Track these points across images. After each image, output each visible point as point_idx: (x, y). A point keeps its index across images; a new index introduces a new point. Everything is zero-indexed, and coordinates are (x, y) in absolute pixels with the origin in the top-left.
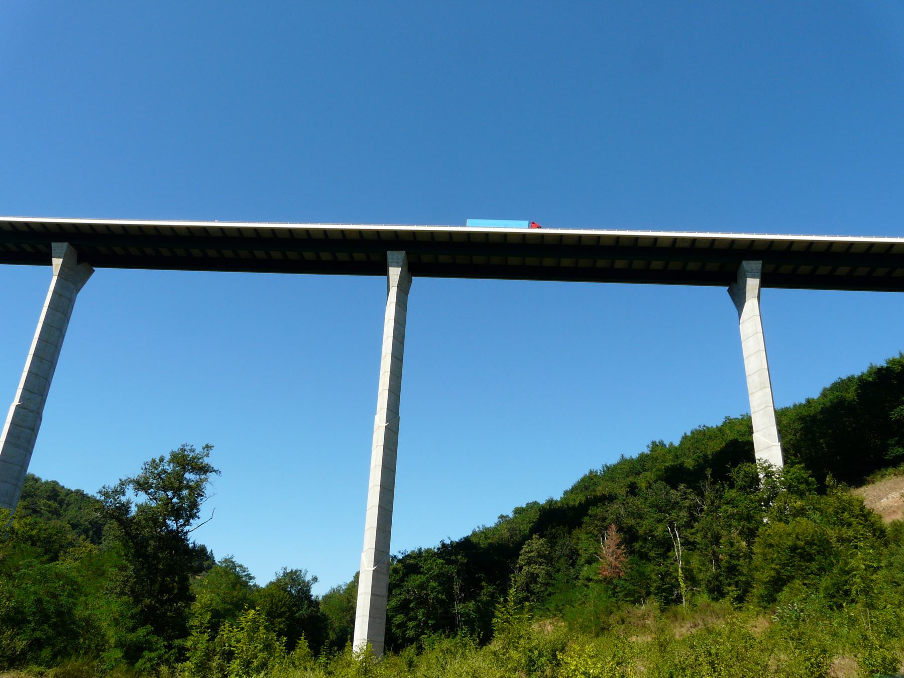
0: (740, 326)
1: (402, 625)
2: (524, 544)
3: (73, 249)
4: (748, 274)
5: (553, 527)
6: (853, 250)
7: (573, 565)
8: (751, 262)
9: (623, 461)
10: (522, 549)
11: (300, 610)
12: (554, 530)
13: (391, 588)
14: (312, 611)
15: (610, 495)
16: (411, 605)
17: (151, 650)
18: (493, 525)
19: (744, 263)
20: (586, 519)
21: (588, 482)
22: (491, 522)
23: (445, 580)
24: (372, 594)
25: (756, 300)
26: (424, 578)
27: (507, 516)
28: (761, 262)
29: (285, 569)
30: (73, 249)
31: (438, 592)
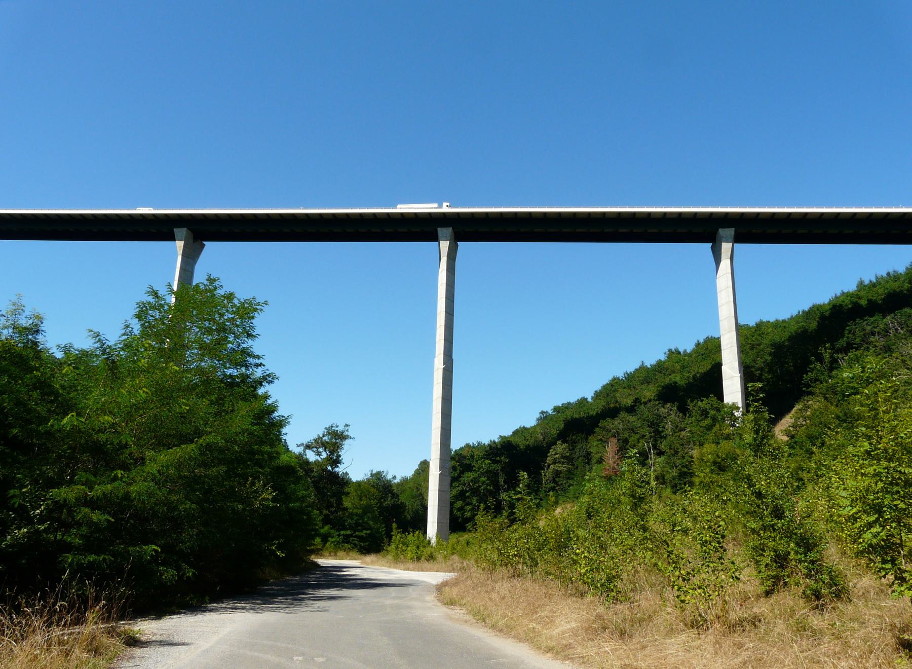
1: (461, 509)
2: (550, 449)
4: (724, 239)
5: (574, 434)
6: (807, 217)
7: (588, 463)
9: (642, 368)
11: (385, 501)
13: (454, 480)
16: (467, 494)
17: (332, 537)
19: (720, 230)
20: (597, 430)
21: (613, 386)
22: (530, 421)
23: (492, 476)
24: (439, 490)
25: (729, 261)
26: (476, 475)
27: (547, 412)
28: (734, 229)
29: (372, 471)
31: (487, 485)
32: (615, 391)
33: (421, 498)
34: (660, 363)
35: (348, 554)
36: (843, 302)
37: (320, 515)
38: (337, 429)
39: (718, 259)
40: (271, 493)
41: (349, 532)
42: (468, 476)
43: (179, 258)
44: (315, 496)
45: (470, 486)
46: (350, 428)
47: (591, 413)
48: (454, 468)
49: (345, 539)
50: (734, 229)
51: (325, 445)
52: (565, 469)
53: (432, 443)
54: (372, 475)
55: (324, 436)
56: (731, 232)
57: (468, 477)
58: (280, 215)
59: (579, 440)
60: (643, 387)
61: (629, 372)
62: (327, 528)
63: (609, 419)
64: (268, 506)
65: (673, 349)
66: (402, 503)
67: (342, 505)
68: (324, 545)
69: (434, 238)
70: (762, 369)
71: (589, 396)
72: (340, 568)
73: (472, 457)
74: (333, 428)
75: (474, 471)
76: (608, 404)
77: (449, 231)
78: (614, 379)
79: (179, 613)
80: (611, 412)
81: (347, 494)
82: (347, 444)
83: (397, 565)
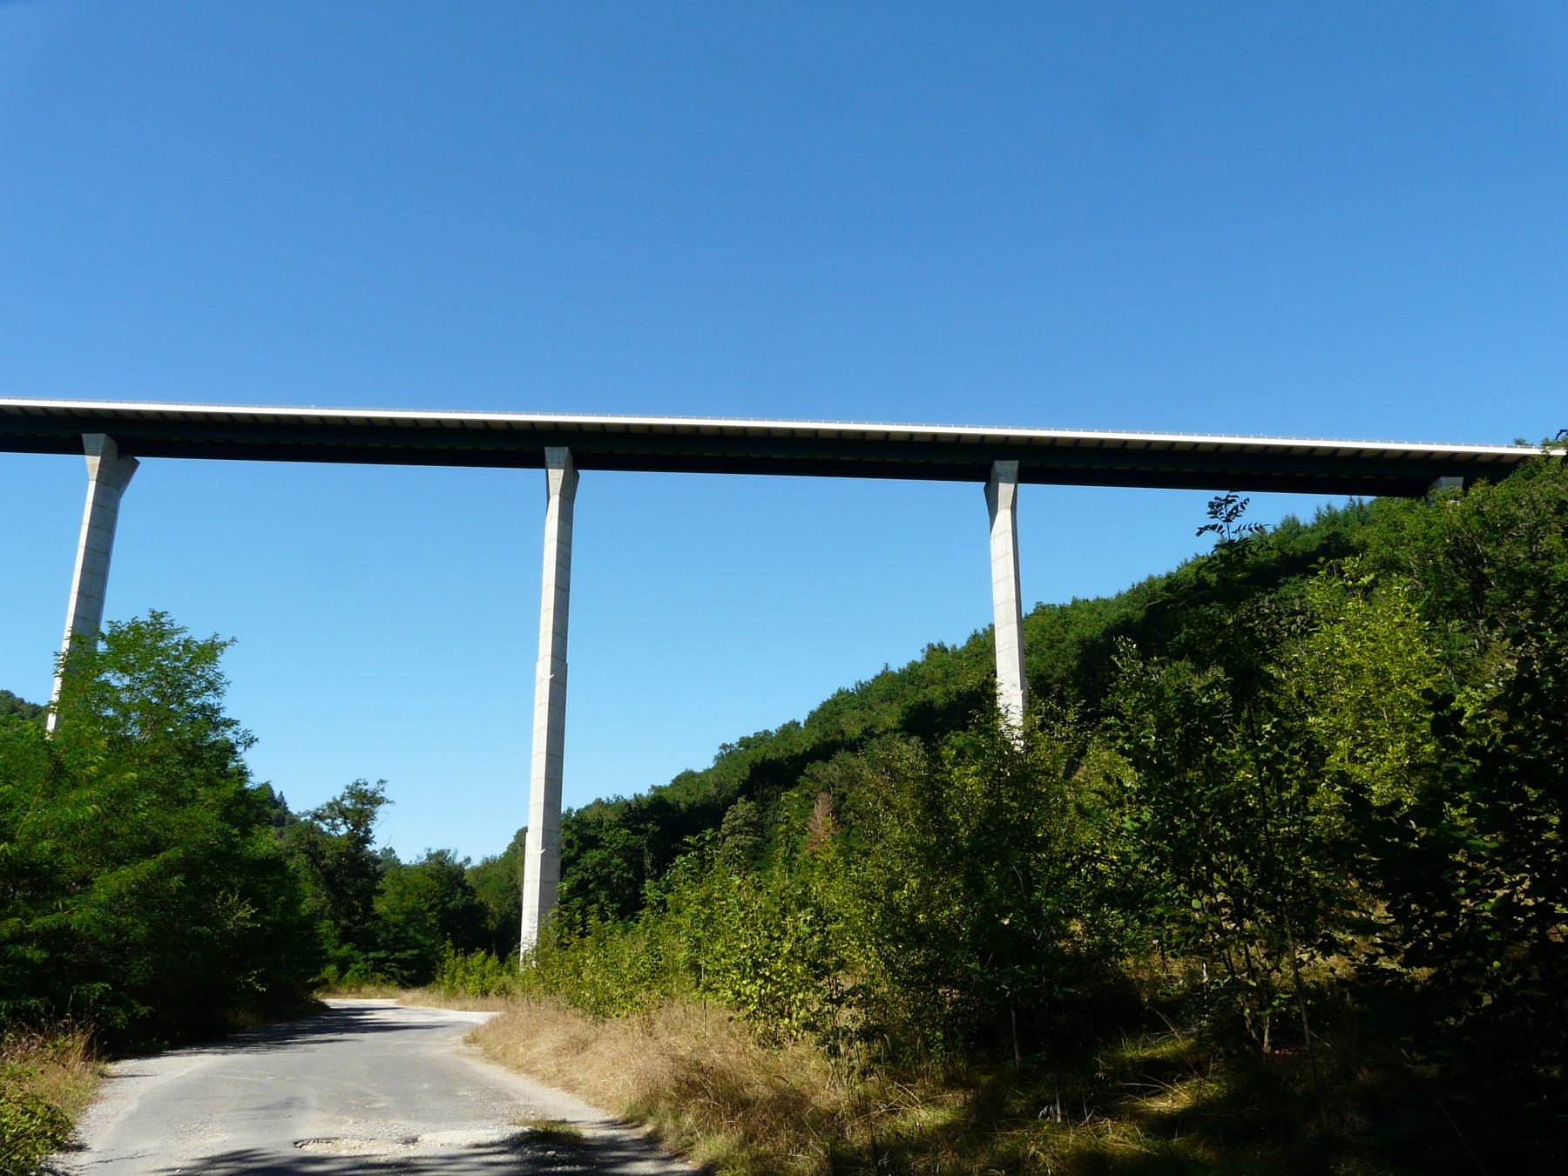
0: (992, 541)
3: (111, 441)
5: (765, 787)
8: (1004, 462)
9: (886, 676)
10: (725, 816)
11: (451, 900)
12: (766, 791)
13: (565, 864)
14: (467, 900)
15: (629, 907)
16: (591, 886)
18: (710, 764)
19: (997, 463)
20: (801, 779)
23: (632, 855)
25: (1009, 511)
28: (1017, 462)
29: (429, 850)
30: (113, 442)
31: (624, 870)
32: (839, 713)
33: (515, 892)
34: (913, 666)
35: (380, 989)
36: (1186, 575)
37: (335, 928)
38: (365, 788)
39: (993, 509)
40: (249, 911)
41: (383, 954)
42: (593, 856)
43: (92, 486)
44: (328, 896)
45: (597, 873)
46: (387, 787)
47: (796, 750)
48: (570, 844)
49: (376, 965)
50: (1017, 462)
51: (344, 813)
52: (749, 843)
53: (531, 803)
54: (430, 857)
55: (343, 799)
56: (1012, 466)
57: (591, 858)
58: (276, 417)
59: (773, 795)
60: (885, 706)
61: (863, 682)
62: (346, 949)
63: (819, 762)
64: (244, 928)
65: (936, 645)
66: (482, 904)
67: (373, 910)
68: (341, 977)
69: (538, 462)
70: (1063, 681)
71: (802, 718)
72: (361, 1011)
73: (600, 823)
74: (359, 787)
75: (603, 846)
76: (826, 734)
77: (562, 453)
78: (840, 692)
79: (134, 1058)
80: (824, 752)
81: (381, 892)
82: (381, 811)
83: (448, 1003)
